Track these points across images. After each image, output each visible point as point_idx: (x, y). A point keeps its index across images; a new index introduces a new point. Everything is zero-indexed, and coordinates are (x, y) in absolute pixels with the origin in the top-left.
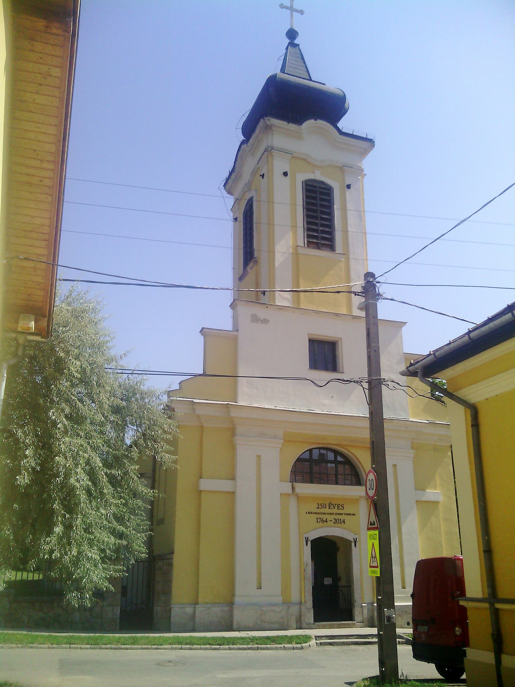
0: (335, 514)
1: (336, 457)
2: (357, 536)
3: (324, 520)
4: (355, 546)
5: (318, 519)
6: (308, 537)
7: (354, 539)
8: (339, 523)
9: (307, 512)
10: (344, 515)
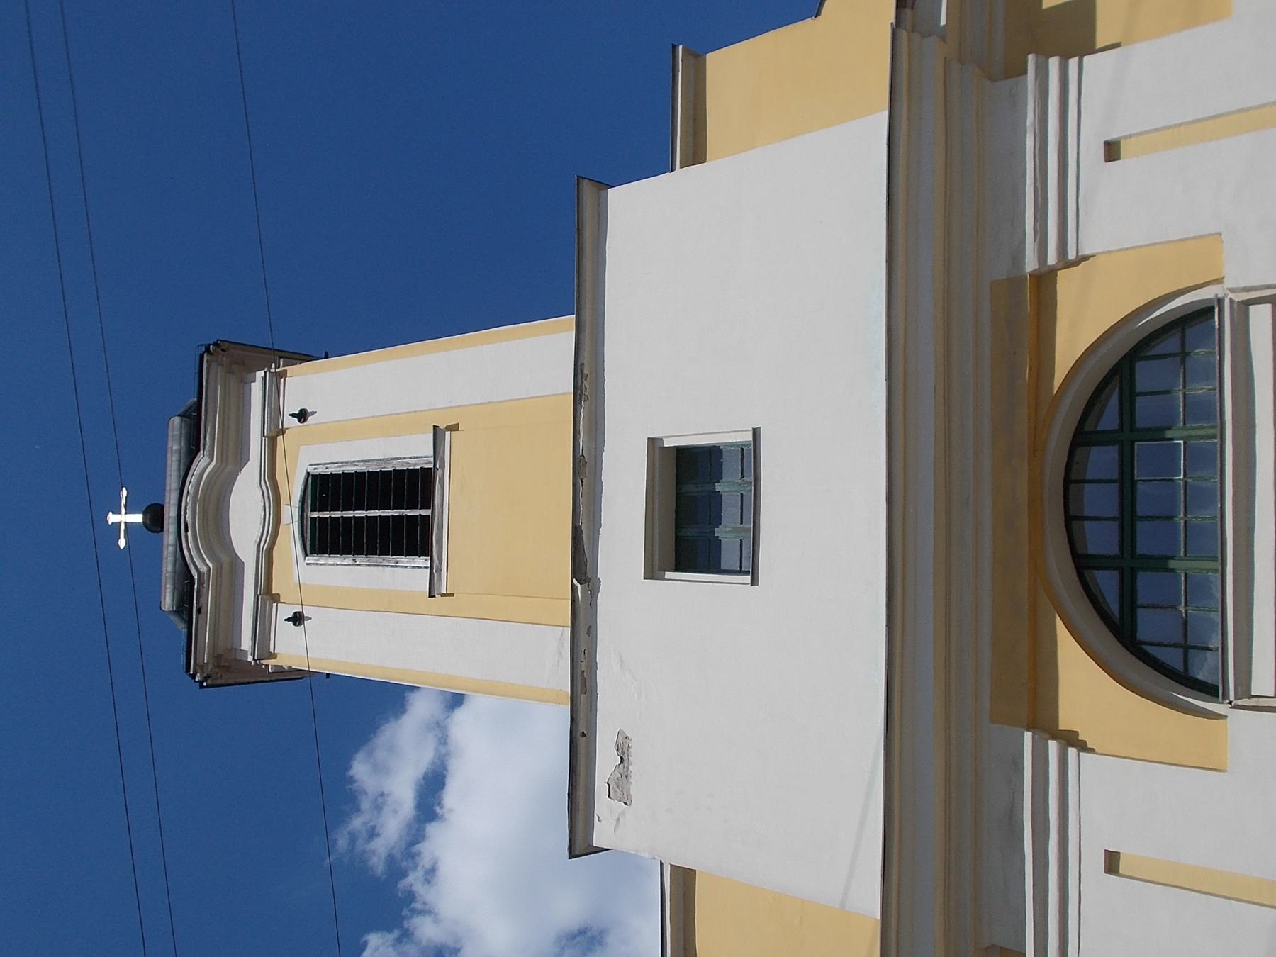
1: (1102, 439)
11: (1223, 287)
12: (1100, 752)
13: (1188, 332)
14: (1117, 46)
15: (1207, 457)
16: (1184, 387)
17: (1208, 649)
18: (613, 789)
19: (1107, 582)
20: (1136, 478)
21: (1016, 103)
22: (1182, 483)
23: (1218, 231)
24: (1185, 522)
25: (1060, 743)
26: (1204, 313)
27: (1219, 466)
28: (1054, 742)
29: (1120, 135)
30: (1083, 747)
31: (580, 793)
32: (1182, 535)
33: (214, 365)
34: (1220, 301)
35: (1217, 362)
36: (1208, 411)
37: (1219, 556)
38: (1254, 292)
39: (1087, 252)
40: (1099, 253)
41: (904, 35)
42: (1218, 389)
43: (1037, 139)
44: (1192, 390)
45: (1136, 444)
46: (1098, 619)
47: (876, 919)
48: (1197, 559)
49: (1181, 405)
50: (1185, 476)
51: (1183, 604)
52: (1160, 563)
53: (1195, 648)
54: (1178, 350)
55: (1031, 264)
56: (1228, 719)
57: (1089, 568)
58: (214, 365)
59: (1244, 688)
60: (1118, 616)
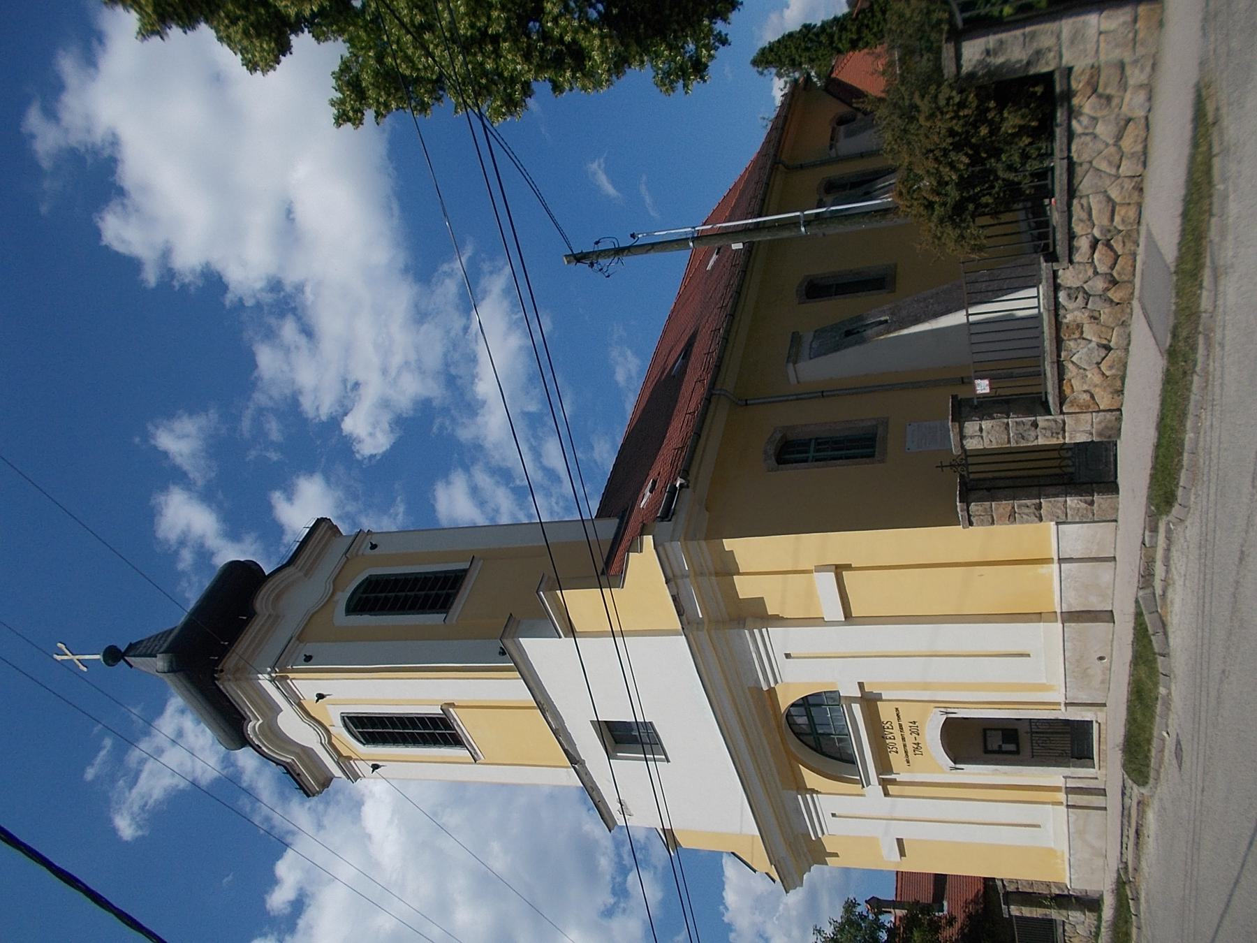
3: (916, 746)
18: (625, 835)
31: (606, 815)
33: (226, 683)
47: (753, 836)
58: (226, 683)
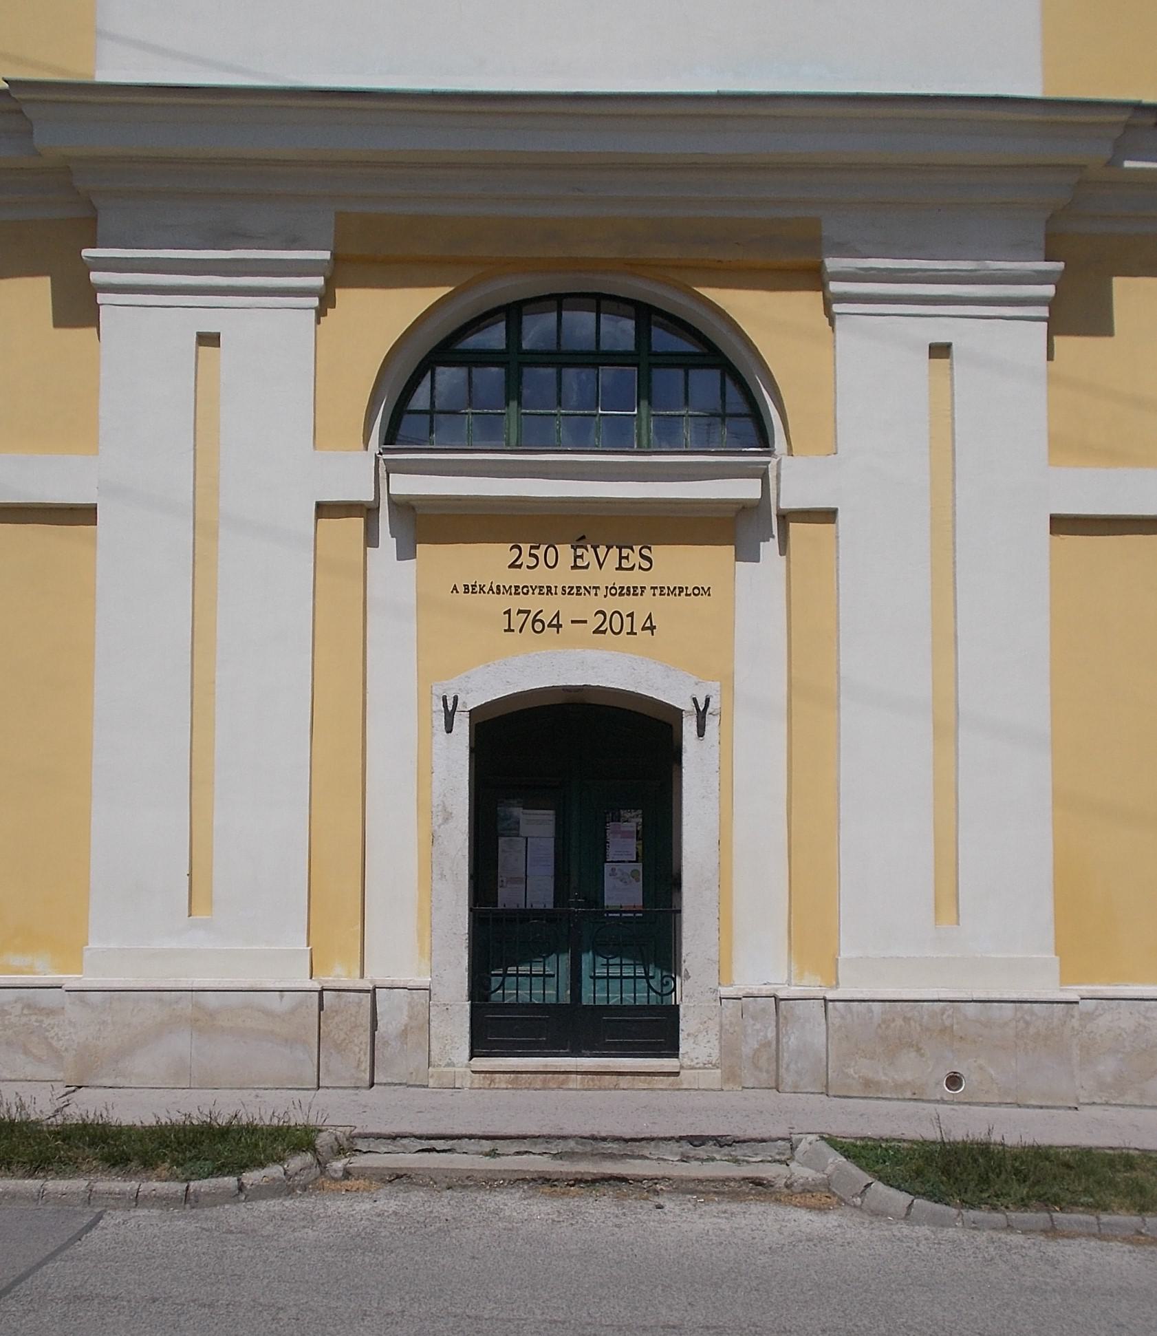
0: (602, 592)
1: (642, 333)
2: (712, 688)
3: (546, 617)
4: (701, 732)
5: (514, 613)
6: (456, 699)
7: (695, 700)
8: (624, 631)
9: (455, 588)
10: (648, 592)
11: (784, 454)
12: (318, 329)
13: (748, 419)
14: (1050, 357)
15: (619, 439)
16: (691, 416)
17: (431, 432)
19: (494, 337)
20: (600, 368)
21: (1017, 250)
22: (594, 412)
23: (839, 452)
24: (555, 415)
25: (321, 289)
26: (764, 439)
27: (608, 449)
28: (323, 283)
29: (954, 359)
30: (321, 312)
32: (542, 411)
34: (769, 454)
35: (709, 449)
36: (668, 437)
37: (520, 448)
38: (775, 482)
39: (837, 323)
40: (835, 336)
41: (1124, 117)
42: (687, 449)
43: (968, 273)
44: (687, 424)
45: (636, 368)
46: (461, 323)
48: (519, 426)
49: (673, 413)
50: (602, 415)
51: (473, 411)
52: (513, 391)
53: (432, 421)
54: (728, 411)
55: (832, 264)
56: (365, 452)
57: (507, 316)
59: (394, 467)
60: (457, 347)
